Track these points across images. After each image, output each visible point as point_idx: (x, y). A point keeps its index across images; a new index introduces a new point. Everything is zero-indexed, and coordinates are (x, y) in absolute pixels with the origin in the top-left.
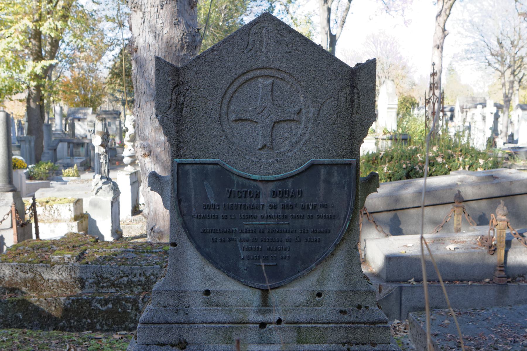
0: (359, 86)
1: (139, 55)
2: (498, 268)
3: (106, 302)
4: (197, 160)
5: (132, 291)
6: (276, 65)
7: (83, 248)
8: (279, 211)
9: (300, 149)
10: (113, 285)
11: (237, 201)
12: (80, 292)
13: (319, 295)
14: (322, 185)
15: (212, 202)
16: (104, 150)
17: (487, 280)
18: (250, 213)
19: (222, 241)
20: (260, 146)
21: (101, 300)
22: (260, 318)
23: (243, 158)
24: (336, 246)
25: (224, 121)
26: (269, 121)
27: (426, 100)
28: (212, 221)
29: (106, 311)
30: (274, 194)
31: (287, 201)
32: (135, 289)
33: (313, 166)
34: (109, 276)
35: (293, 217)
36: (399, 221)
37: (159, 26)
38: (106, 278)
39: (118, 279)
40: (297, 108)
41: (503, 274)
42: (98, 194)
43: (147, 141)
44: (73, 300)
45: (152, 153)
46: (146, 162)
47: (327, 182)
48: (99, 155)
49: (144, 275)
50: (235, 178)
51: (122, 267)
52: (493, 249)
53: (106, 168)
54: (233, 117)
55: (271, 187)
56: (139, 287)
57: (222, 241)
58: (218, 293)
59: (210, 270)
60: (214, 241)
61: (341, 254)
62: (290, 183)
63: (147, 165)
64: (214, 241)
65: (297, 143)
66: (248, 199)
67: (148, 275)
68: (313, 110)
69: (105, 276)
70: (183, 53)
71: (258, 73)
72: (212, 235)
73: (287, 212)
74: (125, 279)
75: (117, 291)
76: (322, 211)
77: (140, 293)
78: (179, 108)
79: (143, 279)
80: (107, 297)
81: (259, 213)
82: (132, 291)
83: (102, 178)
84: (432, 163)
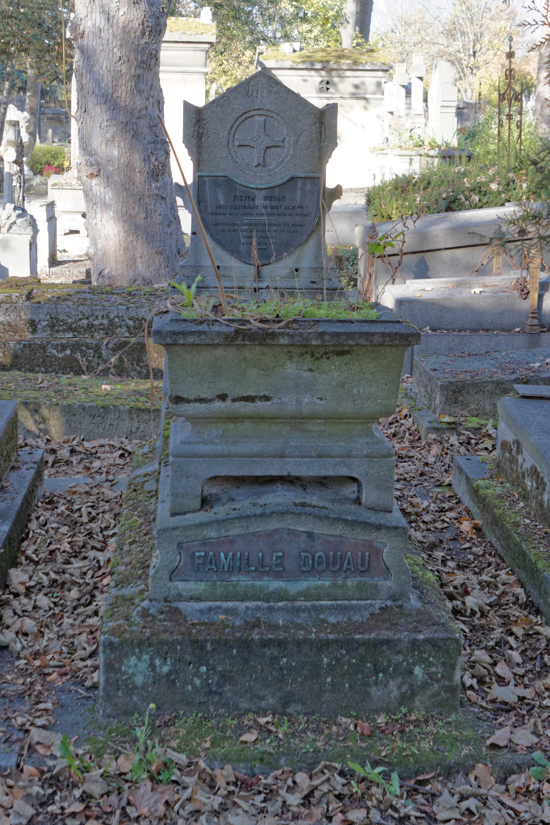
0: (326, 123)
1: (85, 43)
2: (531, 315)
3: (64, 347)
4: (212, 174)
5: (92, 336)
6: (267, 107)
7: (30, 287)
8: (269, 210)
9: (284, 167)
10: (70, 329)
11: (239, 203)
12: (31, 336)
13: (297, 270)
14: (299, 192)
15: (222, 203)
16: (18, 168)
17: (518, 330)
18: (249, 211)
19: (229, 231)
20: (256, 164)
21: (57, 345)
22: (255, 285)
23: (244, 172)
24: (309, 236)
25: (231, 146)
26: (263, 147)
27: (500, 95)
28: (222, 217)
29: (63, 359)
30: (266, 198)
31: (275, 203)
32: (96, 334)
33: (292, 179)
34: (65, 318)
35: (279, 215)
36: (427, 267)
37: (114, 5)
38: (62, 321)
39: (76, 322)
40: (282, 138)
41: (536, 322)
42: (11, 231)
43: (94, 157)
44: (24, 345)
45: (102, 173)
46: (93, 184)
47: (303, 190)
48: (11, 175)
49: (108, 317)
50: (238, 186)
51: (81, 308)
52: (525, 291)
53: (21, 195)
54: (237, 143)
55: (263, 193)
56: (101, 332)
57: (229, 231)
58: (225, 268)
59: (219, 252)
60: (223, 231)
61: (312, 241)
62: (276, 190)
63: (94, 188)
64: (223, 231)
65: (282, 162)
66: (247, 202)
67: (112, 317)
68: (293, 139)
69: (61, 318)
70: (144, 41)
71: (255, 113)
72: (221, 227)
73: (274, 211)
74: (85, 322)
75: (75, 336)
76: (299, 211)
77: (103, 338)
78: (199, 136)
79: (105, 322)
80: (64, 342)
81: (255, 212)
82: (92, 336)
83: (15, 209)
84: (479, 189)
